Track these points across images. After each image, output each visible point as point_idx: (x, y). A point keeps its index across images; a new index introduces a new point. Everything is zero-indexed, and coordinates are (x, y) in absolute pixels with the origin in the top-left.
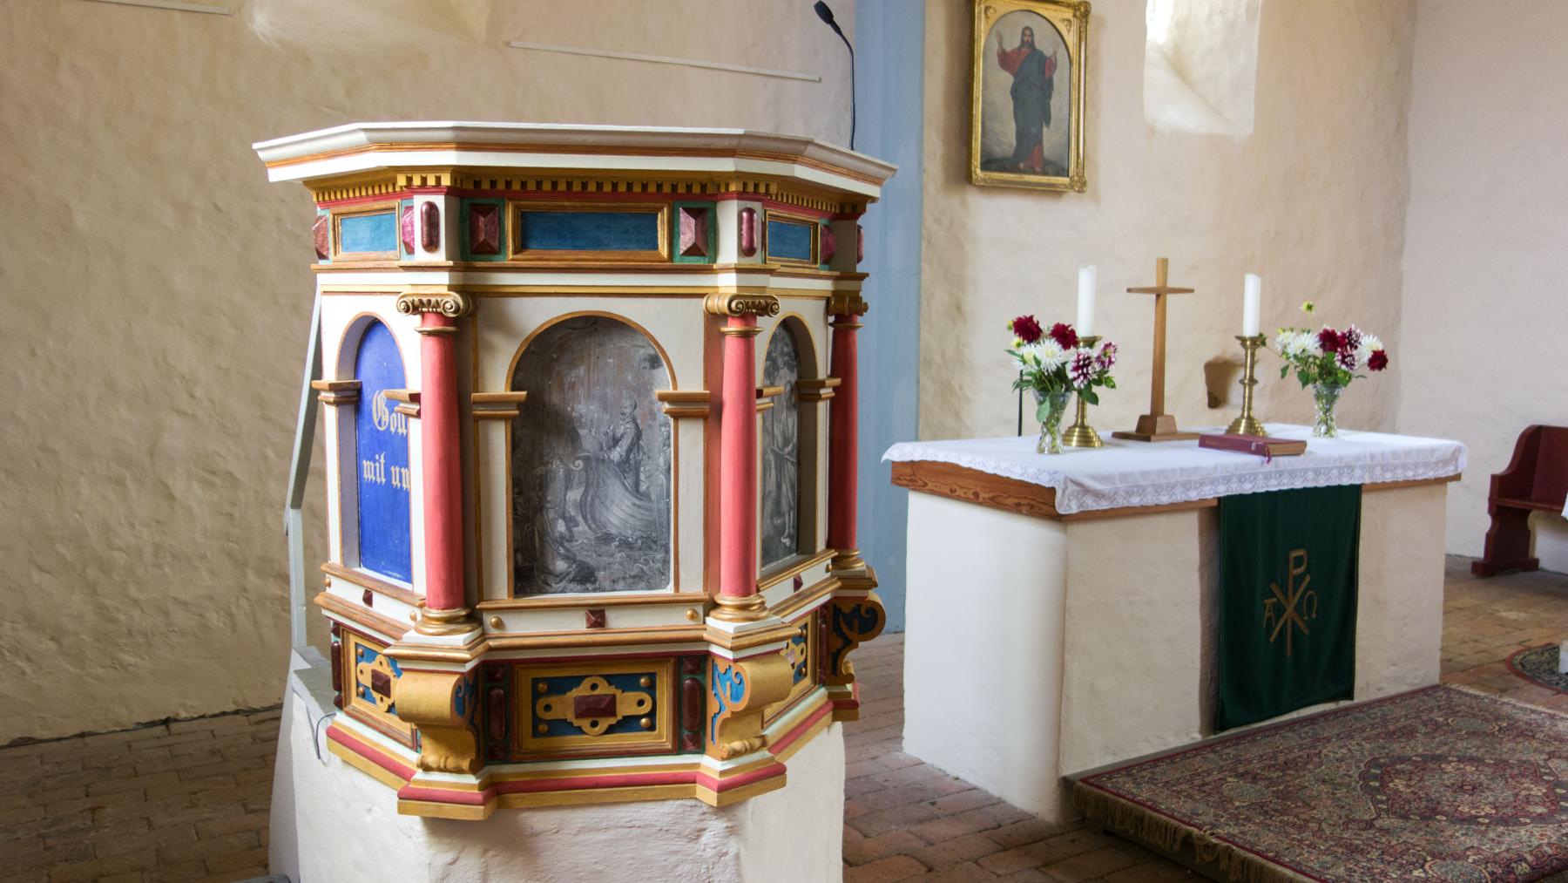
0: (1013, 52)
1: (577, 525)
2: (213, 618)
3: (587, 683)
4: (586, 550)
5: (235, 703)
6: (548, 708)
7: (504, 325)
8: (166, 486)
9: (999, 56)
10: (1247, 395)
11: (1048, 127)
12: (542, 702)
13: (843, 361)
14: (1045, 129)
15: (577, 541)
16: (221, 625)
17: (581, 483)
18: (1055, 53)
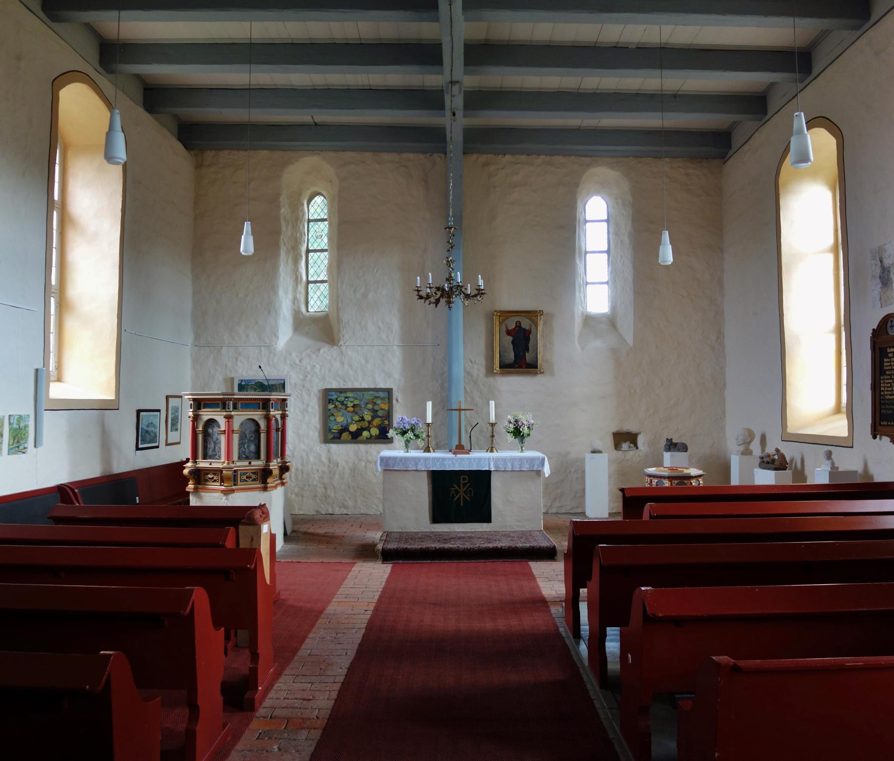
0: (512, 329)
7: (201, 420)
9: (506, 331)
10: (263, 436)
11: (528, 352)
13: (284, 425)
14: (527, 354)
18: (530, 328)
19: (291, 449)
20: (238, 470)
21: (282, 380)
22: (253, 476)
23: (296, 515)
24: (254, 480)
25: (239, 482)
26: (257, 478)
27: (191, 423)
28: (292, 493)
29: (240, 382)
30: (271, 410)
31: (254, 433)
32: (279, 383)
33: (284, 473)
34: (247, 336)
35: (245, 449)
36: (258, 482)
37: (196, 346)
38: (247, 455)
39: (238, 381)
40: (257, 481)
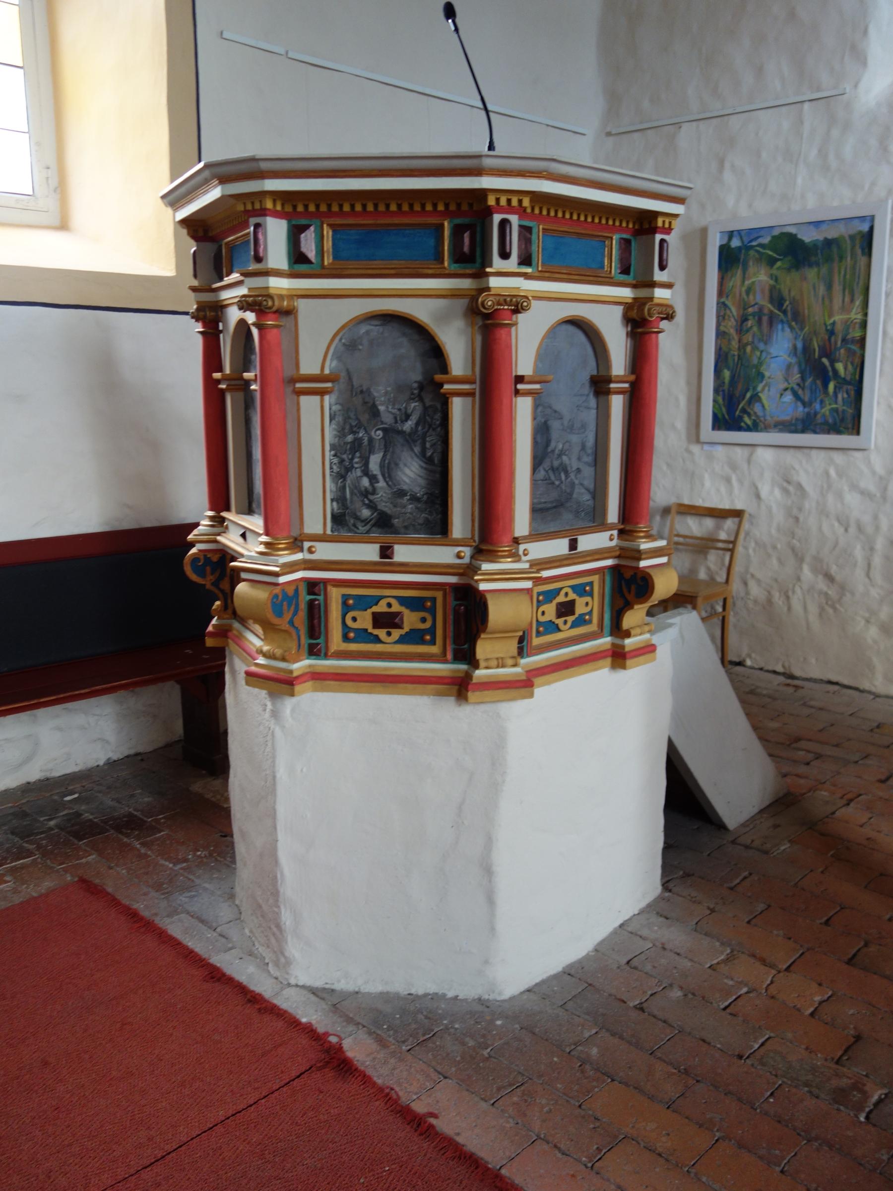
1: (378, 482)
2: (777, 597)
3: (383, 603)
4: (384, 502)
5: (783, 666)
6: (354, 619)
8: (757, 488)
12: (428, 625)
15: (378, 494)
16: (781, 603)
17: (381, 449)
19: (880, 470)
20: (326, 582)
21: (862, 219)
22: (411, 620)
23: (877, 696)
24: (415, 637)
25: (336, 641)
26: (432, 631)
27: (199, 340)
28: (868, 621)
29: (724, 242)
30: (498, 264)
31: (421, 399)
32: (852, 232)
33: (628, 606)
34: (760, 71)
35: (373, 479)
36: (435, 649)
37: (609, 134)
38: (382, 506)
39: (718, 235)
40: (433, 642)
